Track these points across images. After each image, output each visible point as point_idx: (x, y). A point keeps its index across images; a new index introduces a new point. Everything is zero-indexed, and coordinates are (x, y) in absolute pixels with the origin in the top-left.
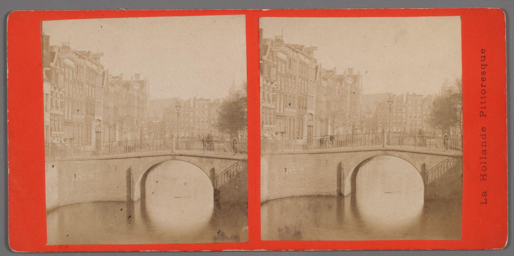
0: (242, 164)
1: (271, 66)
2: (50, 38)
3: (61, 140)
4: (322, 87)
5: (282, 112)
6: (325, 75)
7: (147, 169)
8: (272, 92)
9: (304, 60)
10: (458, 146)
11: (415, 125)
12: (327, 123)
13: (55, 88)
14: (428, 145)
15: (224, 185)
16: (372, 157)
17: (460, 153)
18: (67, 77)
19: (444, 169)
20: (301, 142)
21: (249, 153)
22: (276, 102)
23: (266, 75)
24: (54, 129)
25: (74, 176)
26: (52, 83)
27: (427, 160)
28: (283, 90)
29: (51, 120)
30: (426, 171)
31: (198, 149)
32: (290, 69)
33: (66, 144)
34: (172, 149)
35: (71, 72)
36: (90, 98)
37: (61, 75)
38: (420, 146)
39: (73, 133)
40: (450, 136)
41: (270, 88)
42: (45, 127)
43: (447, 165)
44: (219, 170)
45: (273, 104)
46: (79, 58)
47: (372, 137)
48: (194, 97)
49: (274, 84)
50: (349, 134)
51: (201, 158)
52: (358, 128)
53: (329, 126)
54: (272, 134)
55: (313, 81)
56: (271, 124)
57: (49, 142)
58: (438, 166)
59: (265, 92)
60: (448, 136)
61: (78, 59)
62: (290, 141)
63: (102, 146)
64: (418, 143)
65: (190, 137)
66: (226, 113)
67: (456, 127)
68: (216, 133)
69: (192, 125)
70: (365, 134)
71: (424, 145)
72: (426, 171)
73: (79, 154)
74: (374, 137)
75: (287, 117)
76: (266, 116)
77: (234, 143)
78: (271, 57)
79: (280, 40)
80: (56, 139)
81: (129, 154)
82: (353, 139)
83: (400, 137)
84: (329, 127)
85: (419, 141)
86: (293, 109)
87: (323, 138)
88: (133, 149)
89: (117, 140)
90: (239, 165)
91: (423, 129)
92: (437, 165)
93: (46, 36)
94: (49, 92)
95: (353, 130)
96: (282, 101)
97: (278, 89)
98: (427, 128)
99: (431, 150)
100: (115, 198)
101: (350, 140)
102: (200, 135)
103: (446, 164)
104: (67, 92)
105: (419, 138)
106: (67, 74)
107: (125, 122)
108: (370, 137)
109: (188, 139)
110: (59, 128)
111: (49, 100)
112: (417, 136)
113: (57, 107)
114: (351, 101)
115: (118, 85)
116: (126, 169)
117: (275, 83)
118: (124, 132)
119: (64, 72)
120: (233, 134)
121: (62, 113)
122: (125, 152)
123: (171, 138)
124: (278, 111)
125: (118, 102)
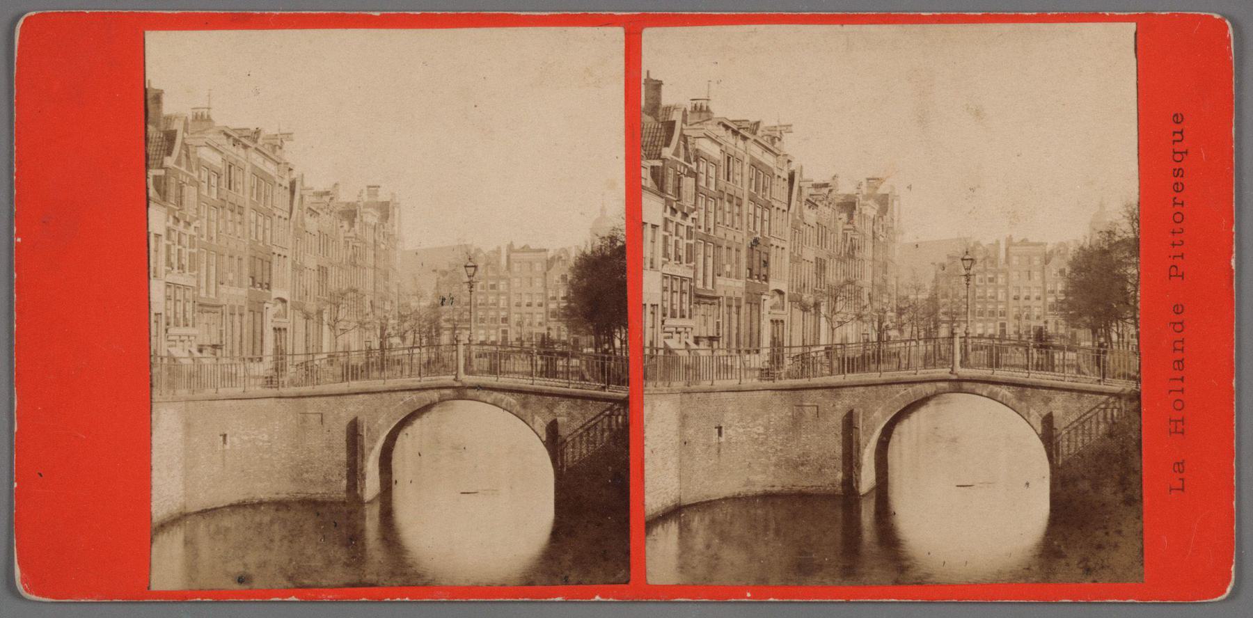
0: (1117, 405)
1: (184, 183)
2: (663, 87)
4: (805, 224)
8: (188, 245)
10: (1129, 369)
11: (1028, 317)
12: (817, 313)
13: (177, 220)
18: (205, 193)
19: (602, 435)
20: (261, 369)
22: (199, 270)
23: (671, 195)
24: (174, 323)
25: (717, 430)
26: (169, 207)
28: (712, 231)
29: (168, 298)
30: (1054, 431)
31: (518, 374)
32: (728, 180)
33: (699, 351)
34: (953, 366)
35: (712, 172)
37: (689, 178)
38: (1040, 368)
39: (219, 332)
40: (1111, 343)
41: (680, 227)
42: (153, 318)
43: (610, 422)
44: (568, 426)
45: (687, 266)
46: (234, 145)
47: (924, 348)
49: (689, 219)
50: (870, 341)
52: (891, 325)
53: (823, 320)
54: (688, 341)
55: (784, 211)
56: (187, 325)
57: (163, 355)
58: (586, 427)
59: (172, 247)
60: (1105, 344)
62: (729, 358)
63: (288, 365)
64: (1035, 362)
66: (585, 283)
67: (1124, 323)
69: (1001, 307)
70: (908, 340)
71: (1050, 367)
73: (730, 377)
75: (224, 308)
77: (603, 358)
78: (184, 159)
79: (206, 117)
80: (676, 336)
81: (355, 385)
82: (879, 352)
86: (727, 277)
87: (808, 351)
88: (362, 371)
89: (326, 348)
90: (1111, 406)
91: (1046, 328)
92: (1080, 418)
93: (153, 89)
94: (162, 231)
95: (881, 331)
96: (710, 261)
98: (1055, 326)
99: (1066, 380)
100: (320, 492)
103: (1101, 414)
104: (206, 232)
105: (1037, 351)
106: (703, 177)
107: (344, 306)
110: (681, 310)
111: (163, 249)
112: (1032, 344)
113: (181, 267)
114: (873, 259)
115: (327, 214)
116: (344, 423)
117: (692, 215)
119: (197, 180)
120: (602, 337)
121: (193, 283)
122: (839, 373)
124: (203, 293)
125: (825, 247)
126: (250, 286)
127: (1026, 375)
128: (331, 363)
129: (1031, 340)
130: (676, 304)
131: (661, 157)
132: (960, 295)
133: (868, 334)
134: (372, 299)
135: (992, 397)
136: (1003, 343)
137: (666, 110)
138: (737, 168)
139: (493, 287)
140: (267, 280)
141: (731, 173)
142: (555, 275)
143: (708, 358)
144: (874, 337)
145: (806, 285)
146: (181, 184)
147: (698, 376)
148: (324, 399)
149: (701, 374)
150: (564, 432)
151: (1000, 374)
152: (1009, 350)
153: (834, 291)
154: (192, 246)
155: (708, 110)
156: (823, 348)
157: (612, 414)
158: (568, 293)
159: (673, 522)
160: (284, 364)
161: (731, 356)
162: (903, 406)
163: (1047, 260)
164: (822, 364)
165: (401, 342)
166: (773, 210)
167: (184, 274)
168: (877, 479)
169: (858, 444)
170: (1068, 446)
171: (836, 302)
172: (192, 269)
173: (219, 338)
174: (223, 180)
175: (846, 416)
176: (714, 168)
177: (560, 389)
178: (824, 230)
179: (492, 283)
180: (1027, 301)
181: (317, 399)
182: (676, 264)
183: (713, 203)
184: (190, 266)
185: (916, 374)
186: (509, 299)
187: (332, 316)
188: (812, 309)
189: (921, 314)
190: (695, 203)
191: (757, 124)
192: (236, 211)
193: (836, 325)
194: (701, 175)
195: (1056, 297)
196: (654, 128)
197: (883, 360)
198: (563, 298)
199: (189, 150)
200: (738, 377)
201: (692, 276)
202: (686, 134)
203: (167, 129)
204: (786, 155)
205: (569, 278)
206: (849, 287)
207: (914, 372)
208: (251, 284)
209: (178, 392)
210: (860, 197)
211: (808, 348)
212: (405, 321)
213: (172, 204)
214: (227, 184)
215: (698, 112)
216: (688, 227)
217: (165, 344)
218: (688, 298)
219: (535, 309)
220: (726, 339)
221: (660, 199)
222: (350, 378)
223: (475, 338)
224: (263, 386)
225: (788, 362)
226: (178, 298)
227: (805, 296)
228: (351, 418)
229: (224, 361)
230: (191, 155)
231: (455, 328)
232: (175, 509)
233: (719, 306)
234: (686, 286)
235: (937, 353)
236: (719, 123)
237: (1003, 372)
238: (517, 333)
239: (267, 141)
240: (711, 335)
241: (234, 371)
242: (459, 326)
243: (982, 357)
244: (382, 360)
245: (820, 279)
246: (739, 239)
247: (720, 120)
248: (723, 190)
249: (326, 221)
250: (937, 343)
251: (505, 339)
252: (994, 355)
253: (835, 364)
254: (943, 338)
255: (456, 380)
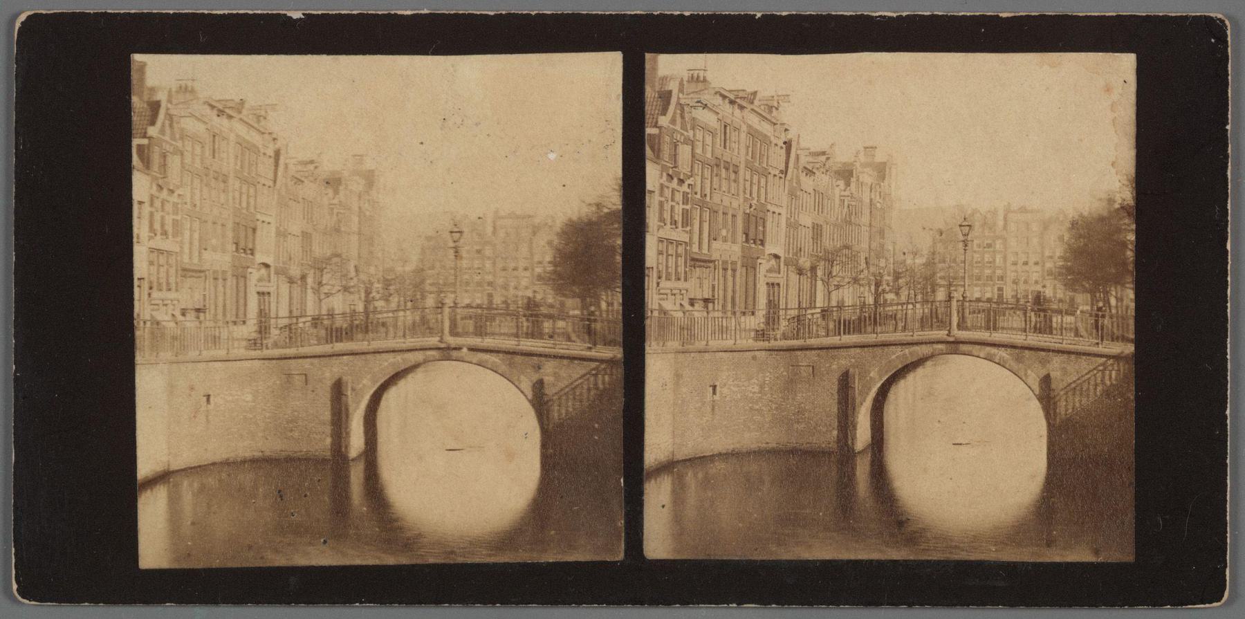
1: (678, 141)
3: (174, 313)
4: (802, 190)
5: (196, 261)
6: (809, 163)
7: (382, 381)
8: (171, 212)
9: (758, 128)
11: (1026, 282)
13: (160, 188)
14: (1056, 329)
15: (1070, 417)
16: (921, 359)
17: (1130, 348)
19: (1095, 389)
20: (753, 324)
21: (1138, 342)
22: (692, 225)
25: (711, 388)
27: (1055, 366)
31: (1013, 330)
32: (725, 147)
36: (244, 211)
37: (686, 146)
41: (666, 189)
42: (136, 283)
43: (1103, 377)
47: (921, 311)
48: (1006, 204)
51: (509, 356)
52: (887, 289)
53: (819, 283)
57: (654, 307)
61: (215, 118)
62: (724, 320)
64: (1033, 324)
65: (995, 301)
68: (547, 295)
70: (904, 304)
72: (1052, 395)
74: (926, 311)
75: (717, 263)
76: (667, 262)
79: (190, 89)
81: (340, 347)
82: (875, 314)
83: (989, 311)
84: (310, 296)
85: (1036, 321)
88: (346, 333)
90: (1110, 368)
94: (146, 199)
95: (877, 295)
96: (706, 226)
97: (186, 206)
98: (1054, 291)
101: (870, 317)
102: (1019, 296)
105: (1035, 314)
106: (699, 144)
108: (917, 311)
109: (479, 311)
110: (168, 284)
112: (1029, 308)
118: (325, 293)
119: (692, 138)
121: (686, 238)
122: (327, 341)
123: (438, 308)
124: (695, 248)
125: (822, 212)
126: (234, 252)
127: (1024, 338)
128: (315, 325)
129: (1029, 304)
130: (672, 267)
131: (148, 136)
132: (957, 259)
133: (864, 297)
134: (357, 263)
135: (989, 358)
136: (1001, 306)
137: (663, 80)
138: (734, 136)
139: (989, 246)
140: (250, 246)
141: (728, 141)
142: (542, 240)
143: (703, 319)
144: (871, 300)
145: (802, 249)
146: (164, 153)
147: (692, 336)
148: (308, 360)
149: (696, 335)
150: (550, 391)
151: (997, 336)
152: (1007, 313)
153: (830, 255)
154: (176, 212)
155: (705, 80)
156: (819, 310)
157: (1105, 369)
158: (1066, 252)
159: (666, 477)
160: (268, 327)
161: (727, 318)
162: (900, 366)
163: (1046, 226)
164: (818, 326)
165: (895, 298)
166: (770, 177)
167: (678, 230)
168: (366, 443)
169: (347, 410)
170: (1066, 406)
171: (832, 266)
172: (175, 235)
173: (711, 293)
174: (718, 140)
175: (842, 375)
176: (711, 136)
177: (547, 349)
178: (821, 197)
179: (478, 248)
180: (515, 271)
181: (300, 361)
182: (162, 239)
183: (710, 171)
184: (683, 223)
185: (912, 336)
186: (1005, 258)
187: (826, 271)
188: (299, 282)
189: (408, 285)
190: (692, 170)
191: (755, 93)
192: (220, 179)
193: (832, 288)
194: (698, 143)
195: (1055, 263)
196: (651, 97)
197: (880, 323)
198: (549, 263)
199: (684, 109)
200: (733, 337)
201: (687, 240)
202: (683, 103)
203: (663, 90)
204: (784, 124)
205: (1066, 238)
206: (335, 260)
207: (911, 333)
208: (744, 240)
209: (669, 344)
210: (858, 164)
211: (295, 319)
212: (390, 285)
213: (155, 172)
214: (723, 143)
215: (696, 82)
216: (684, 192)
217: (656, 297)
218: (683, 261)
219: (521, 273)
220: (721, 302)
221: (146, 177)
222: (842, 333)
223: (968, 295)
224: (247, 348)
225: (783, 323)
226: (670, 252)
227: (801, 261)
228: (337, 377)
229: (208, 324)
230: (175, 125)
231: (950, 285)
232: (159, 468)
233: (715, 269)
234: (681, 249)
235: (934, 316)
236: (716, 93)
237: (1000, 335)
238: (1013, 290)
239: (762, 102)
240: (707, 297)
241: (724, 325)
242: (954, 283)
243: (979, 319)
244: (367, 322)
245: (817, 243)
246: (735, 204)
247: (717, 90)
248: (720, 157)
249: (309, 190)
250: (934, 307)
251: (1000, 296)
252: (992, 319)
253: (831, 326)
254: (940, 301)
255: (441, 341)
